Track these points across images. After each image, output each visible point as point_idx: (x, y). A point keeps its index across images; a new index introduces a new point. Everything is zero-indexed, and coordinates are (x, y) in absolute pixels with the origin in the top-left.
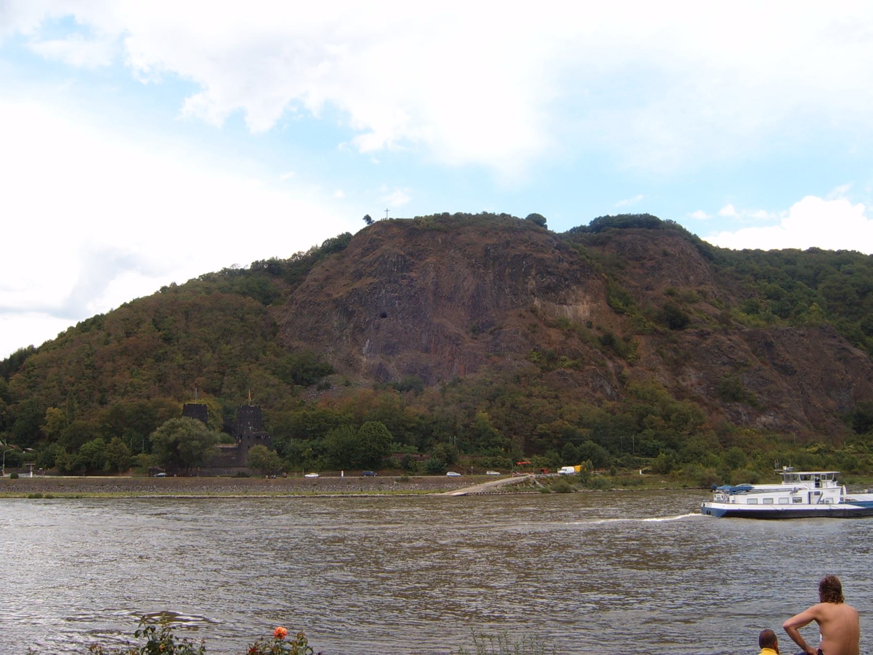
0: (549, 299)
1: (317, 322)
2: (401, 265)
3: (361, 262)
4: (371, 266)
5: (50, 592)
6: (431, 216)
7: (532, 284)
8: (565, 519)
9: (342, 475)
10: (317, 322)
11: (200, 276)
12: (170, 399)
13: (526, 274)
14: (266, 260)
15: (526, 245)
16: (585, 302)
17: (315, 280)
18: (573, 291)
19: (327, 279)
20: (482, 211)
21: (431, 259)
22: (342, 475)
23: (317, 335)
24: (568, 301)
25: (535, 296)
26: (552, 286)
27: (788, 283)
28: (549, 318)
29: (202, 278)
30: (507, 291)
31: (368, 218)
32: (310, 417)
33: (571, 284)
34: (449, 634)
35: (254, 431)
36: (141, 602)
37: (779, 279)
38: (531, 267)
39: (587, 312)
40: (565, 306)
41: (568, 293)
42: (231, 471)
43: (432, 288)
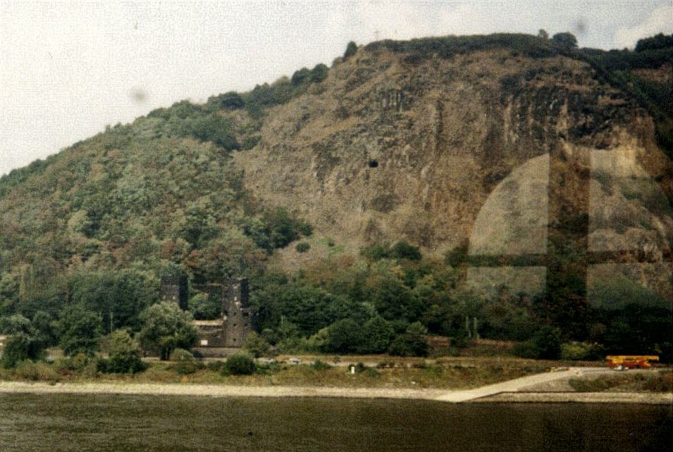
0: (585, 144)
1: (292, 171)
2: (397, 102)
3: (346, 98)
4: (358, 102)
8: (272, 348)
10: (292, 171)
13: (556, 112)
14: (583, 43)
15: (556, 74)
17: (290, 120)
19: (305, 118)
21: (435, 94)
23: (293, 186)
25: (565, 139)
27: (359, 178)
32: (629, 228)
34: (101, 416)
37: (351, 176)
43: (434, 129)
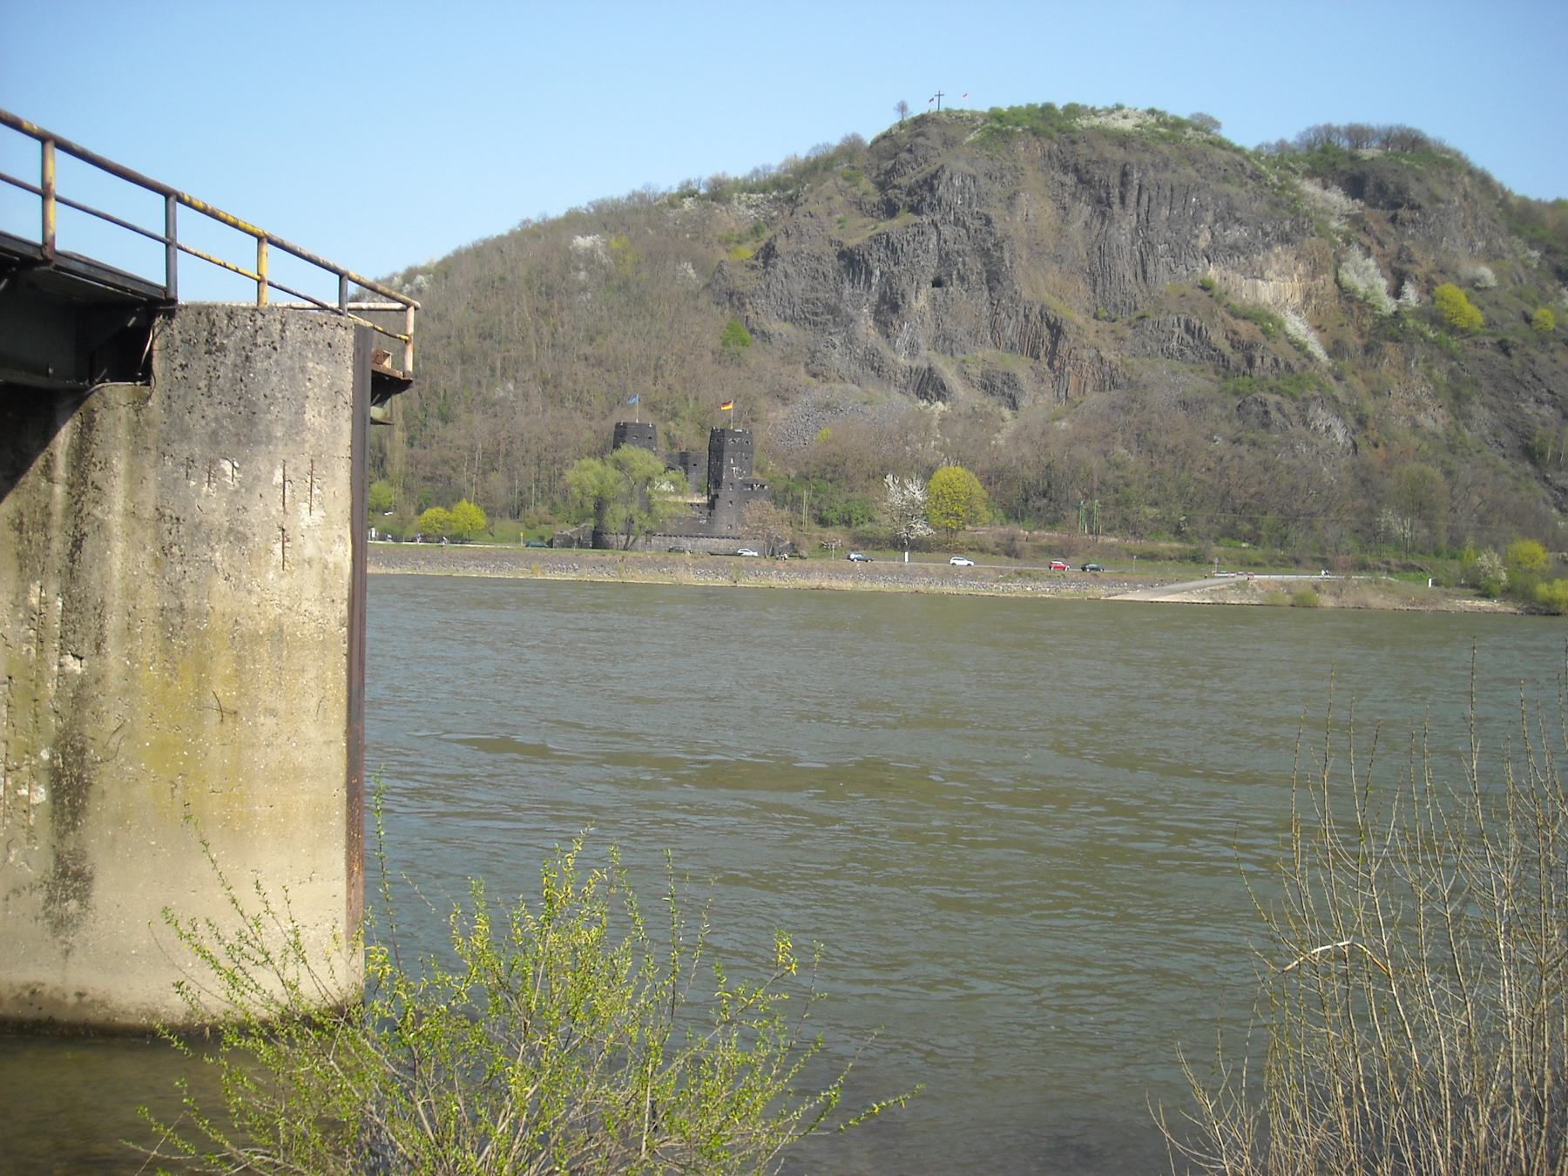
5: (1478, 1130)
6: (1020, 107)
7: (1204, 241)
9: (907, 560)
11: (589, 203)
12: (1262, 533)
13: (1196, 221)
16: (1295, 276)
18: (1277, 256)
20: (989, 107)
22: (907, 560)
24: (1266, 274)
26: (1241, 243)
28: (1236, 303)
29: (594, 207)
30: (1161, 248)
31: (903, 108)
33: (1272, 242)
35: (740, 474)
36: (497, 720)
38: (1203, 207)
39: (1298, 294)
40: (1260, 282)
41: (1267, 259)
42: (699, 543)
